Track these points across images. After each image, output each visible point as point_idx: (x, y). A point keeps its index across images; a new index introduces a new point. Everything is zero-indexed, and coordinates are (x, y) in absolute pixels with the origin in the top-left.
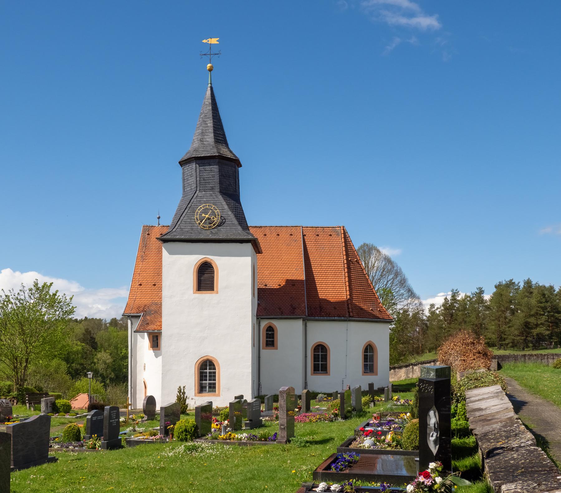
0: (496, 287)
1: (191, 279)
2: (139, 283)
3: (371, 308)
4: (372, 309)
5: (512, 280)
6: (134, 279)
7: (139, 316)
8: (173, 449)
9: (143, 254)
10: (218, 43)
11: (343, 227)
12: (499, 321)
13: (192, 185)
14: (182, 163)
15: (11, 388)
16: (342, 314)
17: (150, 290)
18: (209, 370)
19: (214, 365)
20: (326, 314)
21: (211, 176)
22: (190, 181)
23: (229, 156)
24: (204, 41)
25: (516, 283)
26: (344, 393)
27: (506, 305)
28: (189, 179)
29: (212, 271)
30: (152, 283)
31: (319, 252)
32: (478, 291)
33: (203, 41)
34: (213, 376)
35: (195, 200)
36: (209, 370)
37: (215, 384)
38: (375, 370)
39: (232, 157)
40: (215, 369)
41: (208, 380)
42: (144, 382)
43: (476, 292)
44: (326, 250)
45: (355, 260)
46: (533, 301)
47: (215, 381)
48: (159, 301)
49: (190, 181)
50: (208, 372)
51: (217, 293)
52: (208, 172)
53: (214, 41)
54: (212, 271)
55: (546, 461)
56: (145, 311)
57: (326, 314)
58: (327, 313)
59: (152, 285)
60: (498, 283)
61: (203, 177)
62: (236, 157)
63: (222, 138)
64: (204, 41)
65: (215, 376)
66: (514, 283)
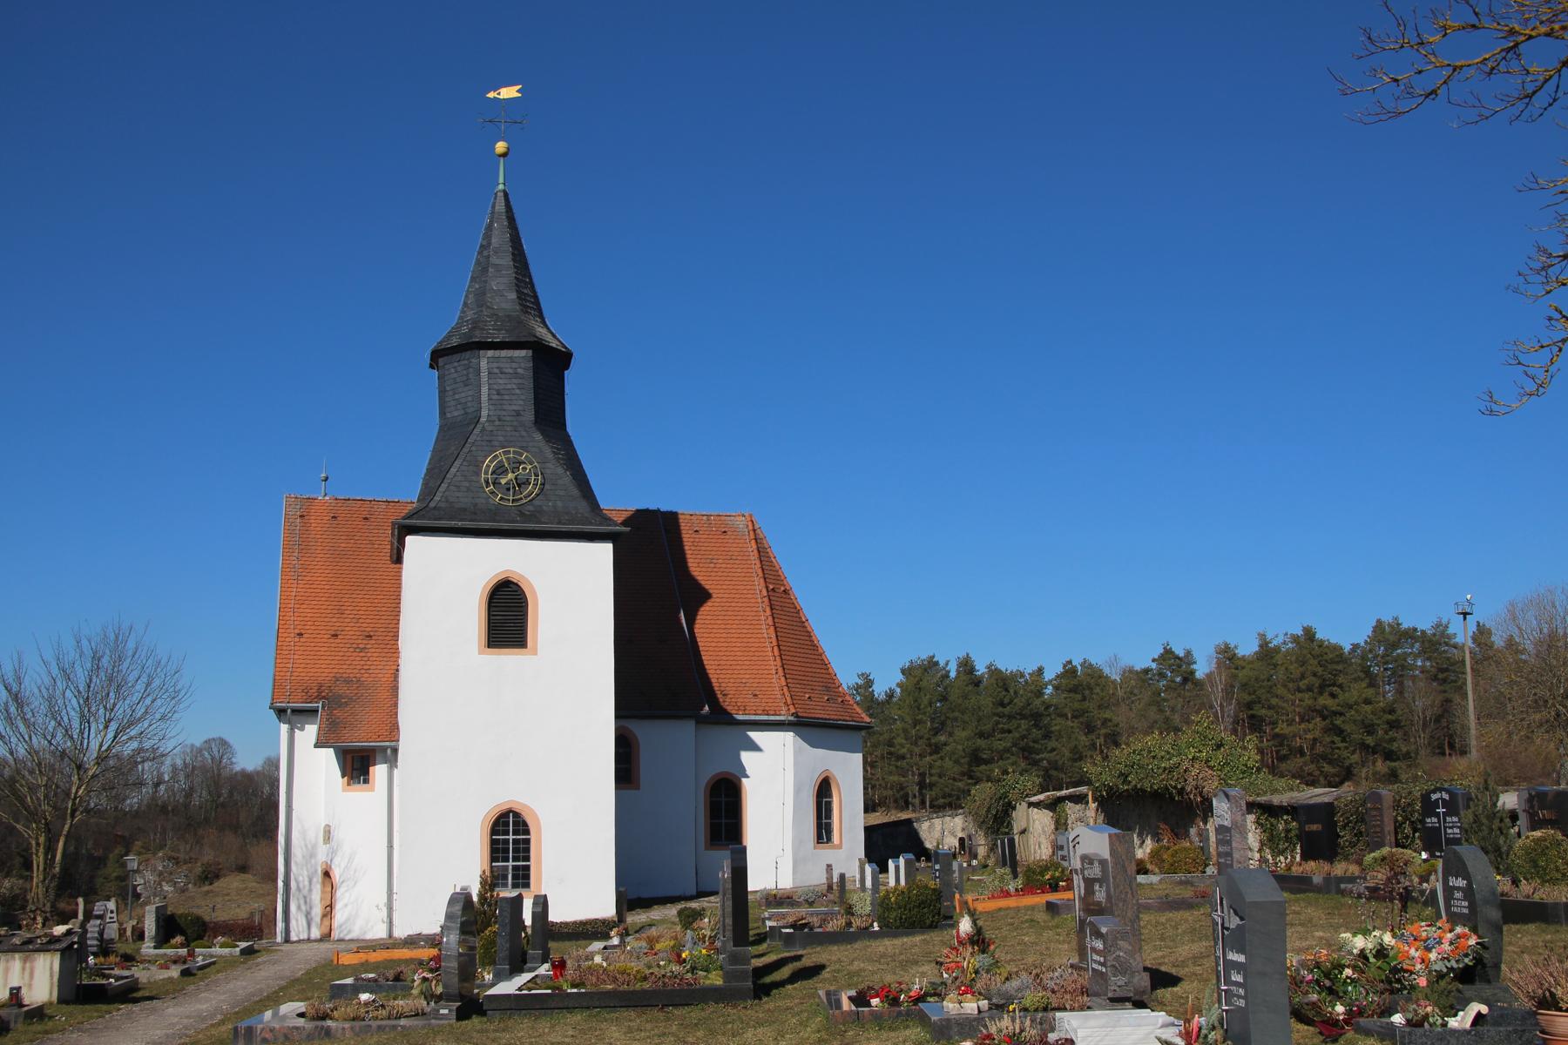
0: (903, 671)
1: (472, 618)
2: (297, 631)
3: (807, 696)
4: (809, 698)
5: (934, 657)
6: (282, 622)
7: (315, 711)
9: (296, 562)
10: (520, 95)
11: (751, 516)
13: (469, 404)
14: (437, 356)
15: (1366, 722)
16: (772, 708)
17: (326, 649)
18: (513, 835)
19: (525, 824)
20: (736, 708)
21: (514, 386)
22: (463, 395)
23: (554, 345)
24: (491, 95)
25: (942, 664)
28: (460, 390)
30: (328, 632)
31: (703, 569)
32: (860, 682)
34: (523, 850)
35: (479, 439)
36: (513, 835)
37: (527, 868)
39: (559, 348)
40: (527, 832)
41: (511, 860)
43: (857, 684)
44: (718, 566)
45: (783, 588)
46: (986, 702)
47: (529, 861)
48: (351, 675)
49: (463, 395)
50: (511, 841)
51: (535, 653)
52: (508, 376)
53: (509, 93)
54: (522, 603)
56: (324, 697)
57: (736, 708)
58: (739, 707)
59: (329, 636)
60: (907, 664)
61: (495, 387)
62: (566, 348)
63: (532, 303)
64: (491, 95)
65: (527, 850)
66: (937, 663)
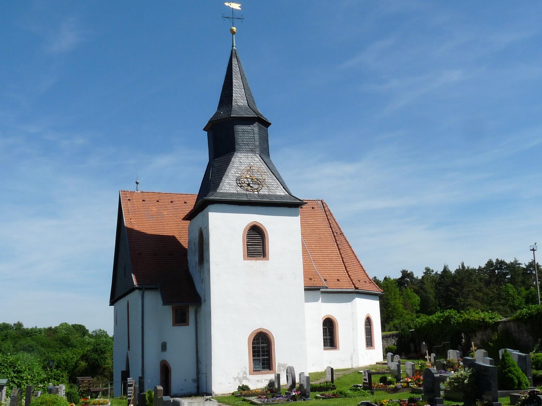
8: (496, 285)
10: (240, 9)
12: (75, 357)
24: (227, 4)
26: (267, 127)
27: (488, 310)
29: (248, 236)
33: (225, 4)
38: (373, 346)
42: (128, 301)
53: (236, 6)
54: (248, 236)
55: (401, 385)
64: (227, 4)
